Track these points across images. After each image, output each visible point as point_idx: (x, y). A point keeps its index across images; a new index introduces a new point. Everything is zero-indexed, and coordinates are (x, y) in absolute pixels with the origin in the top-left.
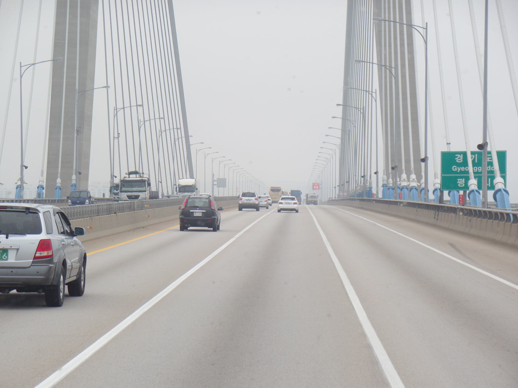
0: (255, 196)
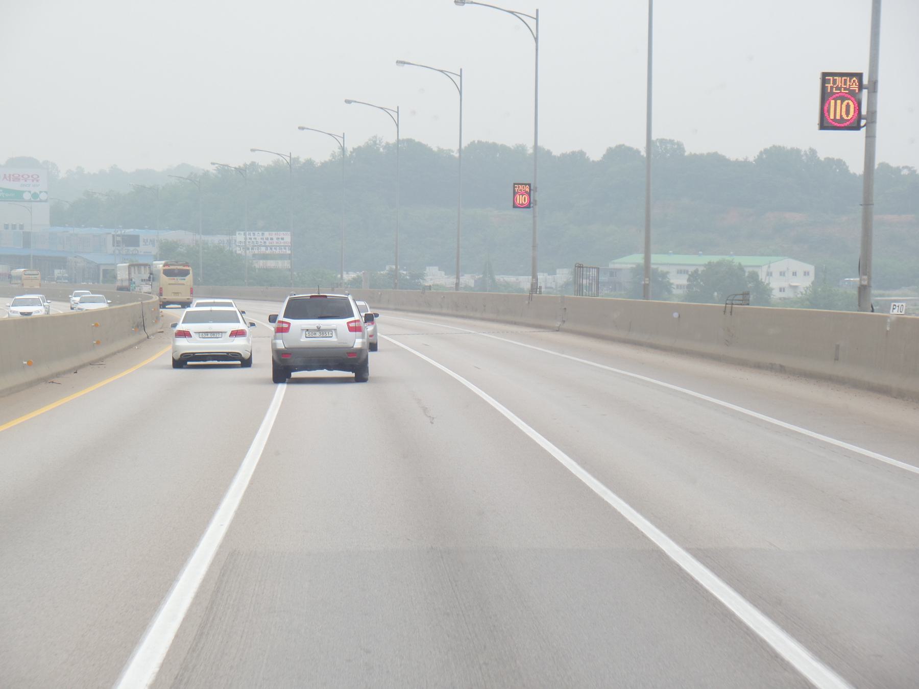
0: (352, 315)
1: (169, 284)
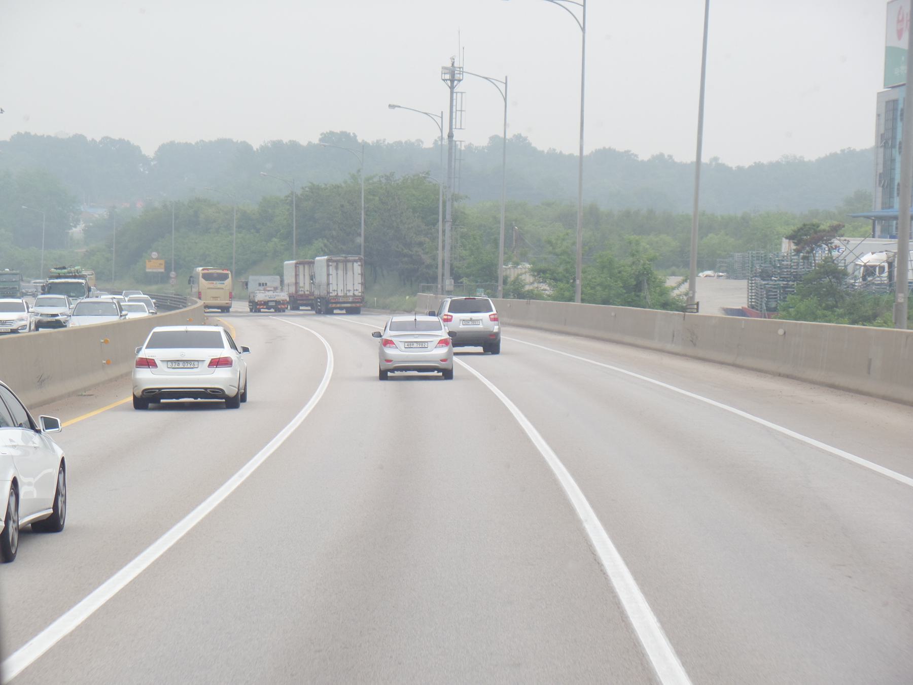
0: (492, 311)
1: (209, 288)
